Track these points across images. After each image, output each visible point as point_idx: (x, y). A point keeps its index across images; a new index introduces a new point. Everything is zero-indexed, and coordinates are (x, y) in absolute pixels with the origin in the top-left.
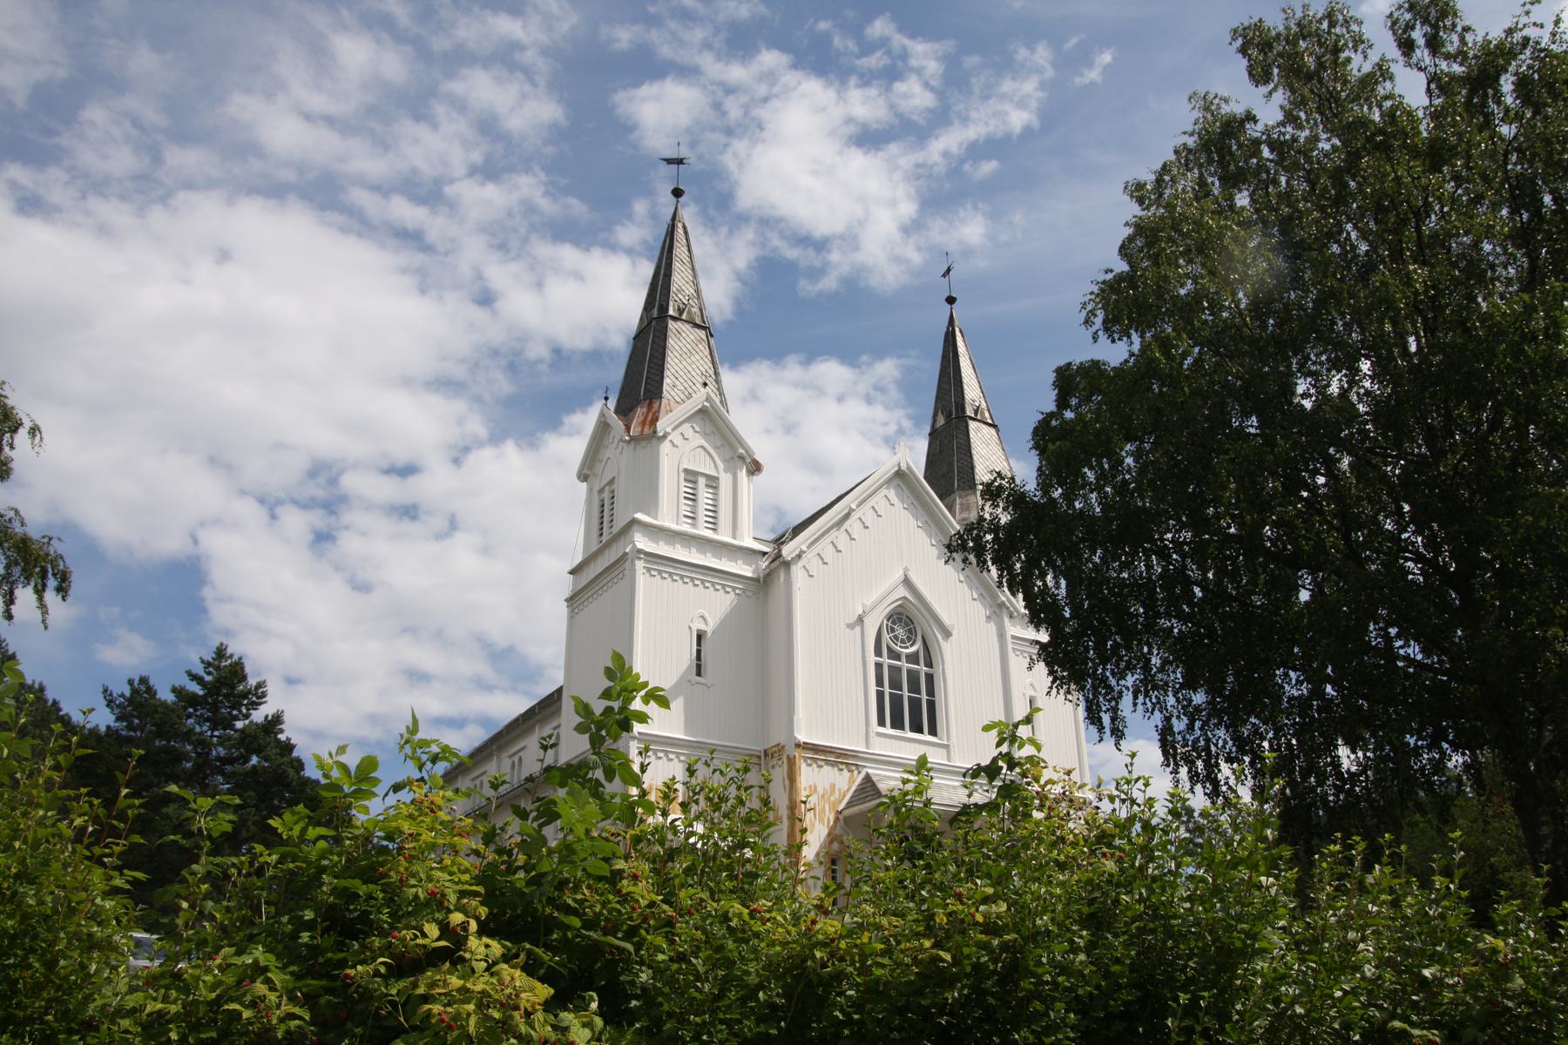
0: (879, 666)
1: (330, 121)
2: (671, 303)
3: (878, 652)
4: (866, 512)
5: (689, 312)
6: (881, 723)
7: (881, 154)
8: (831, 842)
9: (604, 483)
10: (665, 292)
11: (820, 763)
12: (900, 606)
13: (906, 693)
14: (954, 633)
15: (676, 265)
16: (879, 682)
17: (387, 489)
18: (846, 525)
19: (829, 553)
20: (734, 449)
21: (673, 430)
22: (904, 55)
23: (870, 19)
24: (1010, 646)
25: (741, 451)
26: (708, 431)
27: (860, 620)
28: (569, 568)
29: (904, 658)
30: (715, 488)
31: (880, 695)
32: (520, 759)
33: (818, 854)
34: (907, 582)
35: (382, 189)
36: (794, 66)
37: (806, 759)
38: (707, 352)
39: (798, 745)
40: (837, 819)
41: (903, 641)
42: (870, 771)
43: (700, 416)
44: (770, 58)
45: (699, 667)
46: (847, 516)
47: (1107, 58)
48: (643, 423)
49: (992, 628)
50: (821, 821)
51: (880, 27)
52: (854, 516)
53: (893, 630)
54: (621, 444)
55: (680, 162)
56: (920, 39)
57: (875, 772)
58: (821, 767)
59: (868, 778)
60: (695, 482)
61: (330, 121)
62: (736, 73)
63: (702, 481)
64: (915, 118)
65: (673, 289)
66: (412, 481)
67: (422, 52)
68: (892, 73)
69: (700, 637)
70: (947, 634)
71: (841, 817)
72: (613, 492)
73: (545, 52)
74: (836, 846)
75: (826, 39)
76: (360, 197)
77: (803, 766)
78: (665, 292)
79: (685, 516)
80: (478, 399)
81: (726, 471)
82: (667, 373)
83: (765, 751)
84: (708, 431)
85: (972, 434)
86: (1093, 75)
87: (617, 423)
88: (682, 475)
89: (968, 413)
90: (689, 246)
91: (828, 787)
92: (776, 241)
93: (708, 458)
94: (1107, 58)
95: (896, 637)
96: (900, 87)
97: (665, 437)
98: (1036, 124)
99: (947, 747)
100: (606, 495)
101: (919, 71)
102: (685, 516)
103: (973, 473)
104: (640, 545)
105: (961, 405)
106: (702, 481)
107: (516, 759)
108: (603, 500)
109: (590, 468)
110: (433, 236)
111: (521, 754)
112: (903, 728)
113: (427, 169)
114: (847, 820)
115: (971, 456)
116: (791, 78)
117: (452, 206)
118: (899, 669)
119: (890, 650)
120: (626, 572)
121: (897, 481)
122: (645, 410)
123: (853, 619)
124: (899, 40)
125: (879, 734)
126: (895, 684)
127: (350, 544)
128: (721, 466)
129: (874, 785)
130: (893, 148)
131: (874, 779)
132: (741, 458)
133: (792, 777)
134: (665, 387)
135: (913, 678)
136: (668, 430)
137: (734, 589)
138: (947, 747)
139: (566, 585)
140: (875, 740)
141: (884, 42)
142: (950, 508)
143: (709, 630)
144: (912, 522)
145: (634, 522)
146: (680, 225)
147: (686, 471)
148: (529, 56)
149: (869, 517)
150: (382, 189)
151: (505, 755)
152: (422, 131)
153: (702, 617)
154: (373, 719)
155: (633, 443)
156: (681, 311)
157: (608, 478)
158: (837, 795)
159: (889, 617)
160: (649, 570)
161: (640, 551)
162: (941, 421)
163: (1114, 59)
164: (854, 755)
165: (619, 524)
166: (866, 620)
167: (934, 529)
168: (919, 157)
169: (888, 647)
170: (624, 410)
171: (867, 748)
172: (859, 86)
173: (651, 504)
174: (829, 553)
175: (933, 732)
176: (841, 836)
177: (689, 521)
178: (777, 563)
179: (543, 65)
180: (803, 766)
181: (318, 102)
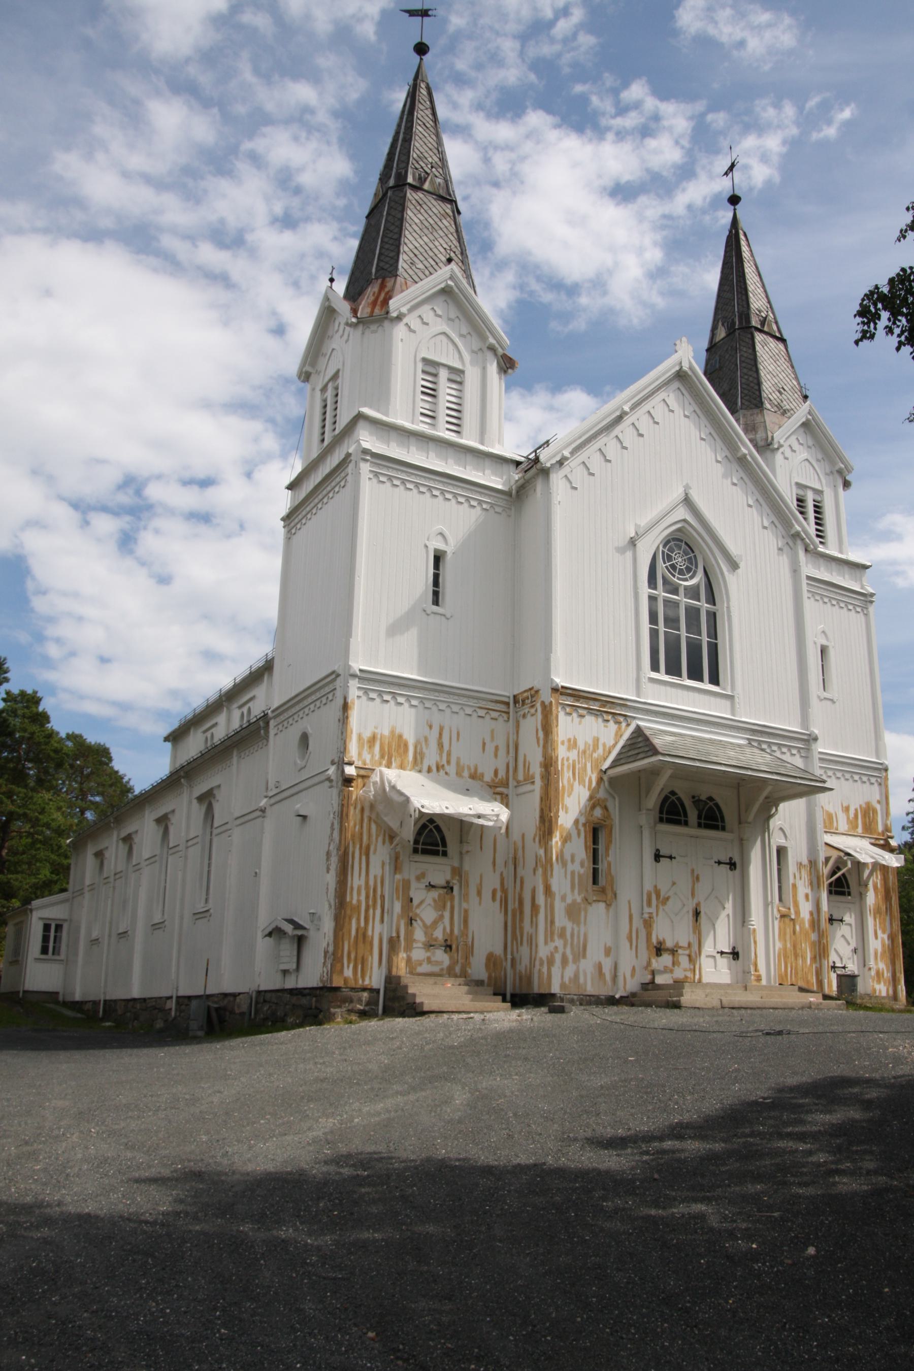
0: (652, 599)
1: (147, 179)
2: (410, 171)
3: (652, 581)
4: (640, 417)
5: (432, 182)
6: (655, 667)
7: (630, 206)
8: (593, 807)
9: (326, 379)
10: (404, 158)
11: (581, 711)
12: (679, 530)
13: (684, 634)
14: (742, 565)
15: (418, 129)
16: (653, 619)
17: (188, 499)
18: (617, 431)
19: (596, 463)
20: (483, 338)
21: (411, 310)
22: (656, 117)
23: (626, 85)
24: (805, 588)
25: (492, 340)
26: (452, 316)
27: (633, 542)
28: (287, 482)
29: (681, 591)
30: (460, 383)
31: (654, 634)
32: (249, 709)
33: (576, 822)
34: (687, 501)
35: (191, 238)
36: (557, 126)
37: (564, 706)
38: (452, 229)
39: (555, 690)
40: (600, 780)
41: (681, 572)
42: (641, 723)
43: (441, 299)
44: (535, 119)
45: (436, 594)
46: (619, 419)
47: (846, 114)
48: (374, 304)
49: (784, 561)
50: (582, 782)
51: (637, 91)
52: (628, 421)
53: (670, 558)
54: (348, 328)
55: (424, 13)
56: (673, 100)
57: (647, 724)
58: (582, 716)
59: (639, 731)
60: (435, 375)
61: (147, 179)
62: (504, 131)
63: (443, 374)
64: (665, 173)
65: (414, 155)
66: (211, 491)
67: (227, 118)
68: (646, 131)
69: (438, 559)
70: (734, 565)
71: (605, 778)
72: (337, 388)
73: (336, 114)
74: (598, 812)
75: (584, 99)
76: (168, 242)
77: (561, 714)
78: (404, 158)
79: (422, 414)
80: (271, 421)
81: (473, 363)
82: (404, 248)
83: (515, 697)
84: (452, 316)
85: (758, 347)
86: (831, 132)
87: (344, 308)
88: (420, 366)
89: (753, 324)
90: (433, 108)
91: (590, 742)
92: (535, 286)
93: (451, 346)
94: (846, 114)
95: (673, 567)
96: (652, 143)
97: (399, 318)
98: (777, 179)
99: (731, 698)
100: (329, 393)
101: (670, 129)
102: (422, 414)
103: (759, 390)
104: (365, 445)
105: (745, 314)
106: (443, 374)
107: (245, 710)
108: (325, 400)
109: (313, 364)
110: (235, 276)
111: (250, 704)
112: (679, 675)
113: (232, 222)
114: (613, 781)
115: (757, 371)
116: (553, 135)
117: (253, 253)
118: (676, 604)
119: (665, 581)
120: (349, 478)
121: (676, 384)
122: (376, 289)
123: (623, 541)
124: (651, 103)
125: (652, 680)
126: (672, 622)
127: (148, 542)
128: (467, 356)
129: (647, 739)
130: (643, 200)
131: (647, 733)
132: (492, 349)
133: (547, 728)
134: (401, 263)
135: (693, 614)
136: (404, 310)
137: (480, 502)
138: (731, 698)
139: (284, 502)
140: (648, 687)
141: (637, 105)
142: (737, 420)
143: (449, 549)
144: (695, 433)
145: (360, 417)
146: (423, 85)
147: (425, 361)
148: (322, 117)
149: (644, 424)
150: (191, 238)
151: (235, 705)
152: (224, 184)
153: (441, 534)
154: (174, 694)
155: (361, 327)
156: (422, 180)
157: (330, 373)
158: (600, 751)
159: (666, 543)
160: (376, 474)
161: (365, 451)
162: (722, 333)
163: (852, 114)
164: (623, 703)
165: (344, 420)
166: (639, 545)
167: (719, 443)
168: (666, 208)
169: (664, 578)
170: (353, 294)
171: (638, 693)
172: (614, 142)
173: (382, 396)
174: (596, 463)
175: (715, 680)
176: (605, 800)
177: (428, 420)
178: (533, 471)
179: (334, 126)
180: (561, 714)
181: (136, 161)
